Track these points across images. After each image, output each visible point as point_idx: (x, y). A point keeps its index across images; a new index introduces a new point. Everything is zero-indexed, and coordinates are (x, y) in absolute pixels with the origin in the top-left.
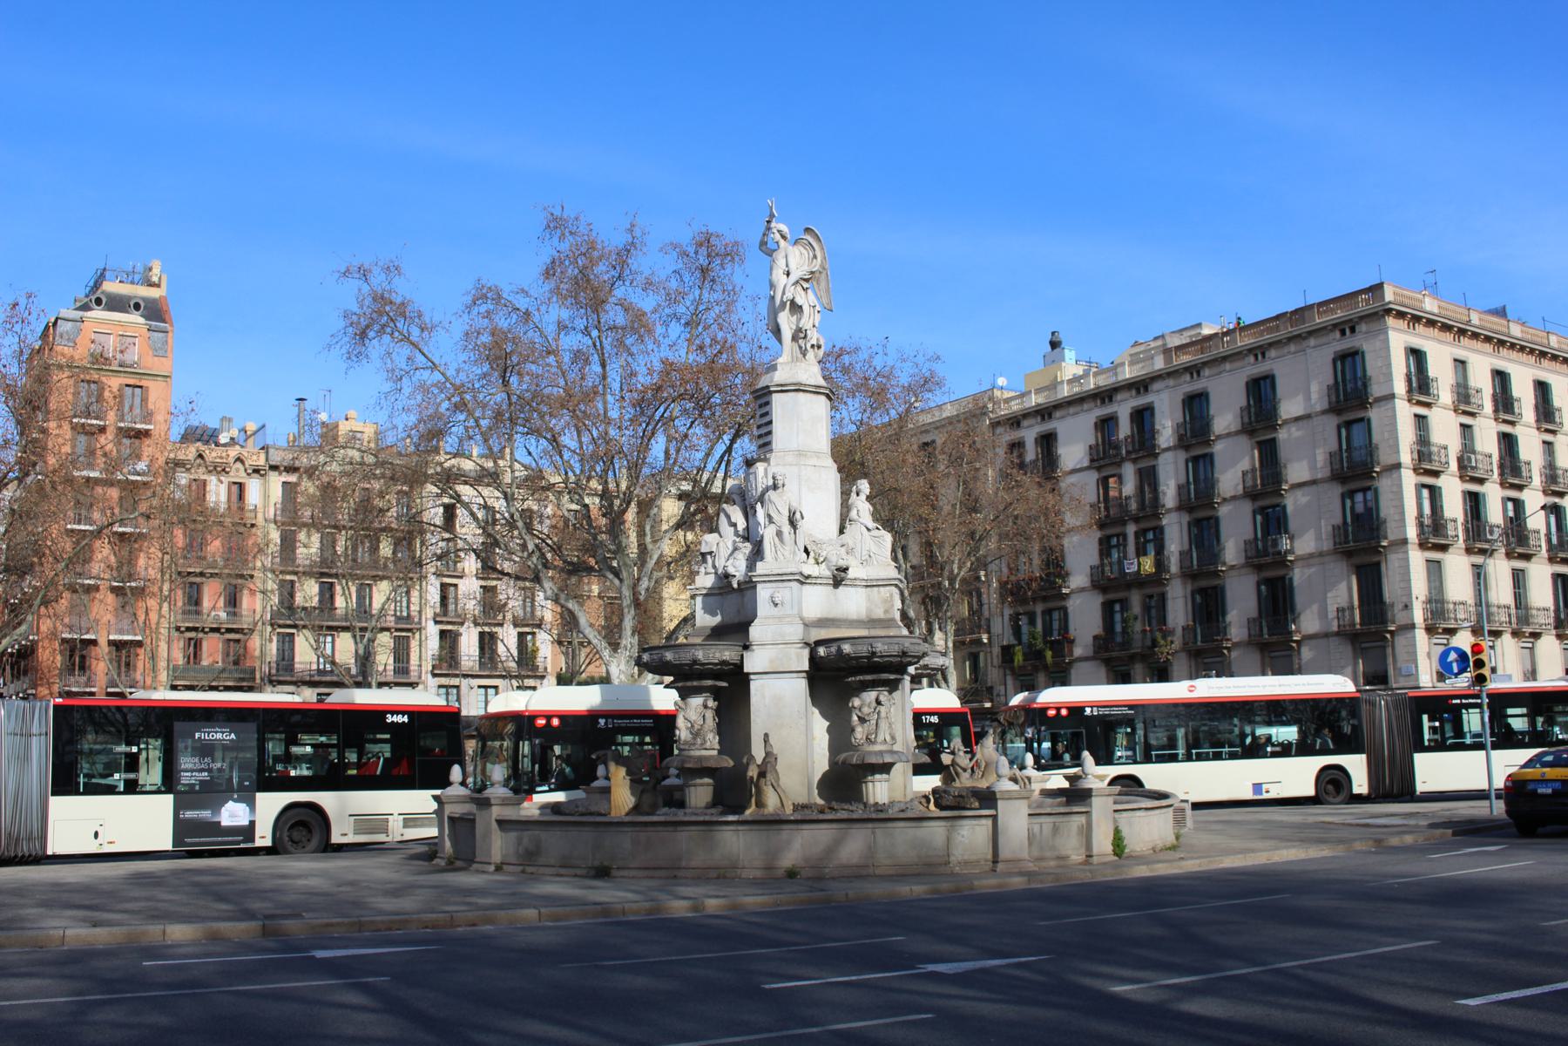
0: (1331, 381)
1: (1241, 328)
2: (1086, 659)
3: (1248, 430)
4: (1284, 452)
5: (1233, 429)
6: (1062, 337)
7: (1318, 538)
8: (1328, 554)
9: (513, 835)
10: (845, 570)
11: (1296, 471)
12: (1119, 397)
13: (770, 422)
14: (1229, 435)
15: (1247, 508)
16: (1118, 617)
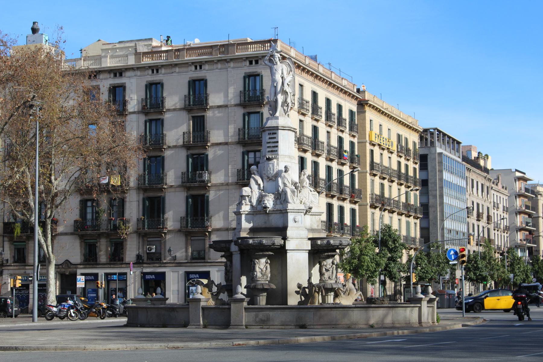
0: (242, 89)
1: (190, 49)
3: (188, 109)
4: (209, 124)
8: (232, 184)
9: (253, 314)
10: (310, 208)
11: (216, 136)
12: (102, 76)
13: (278, 142)
15: (183, 153)
16: (89, 210)
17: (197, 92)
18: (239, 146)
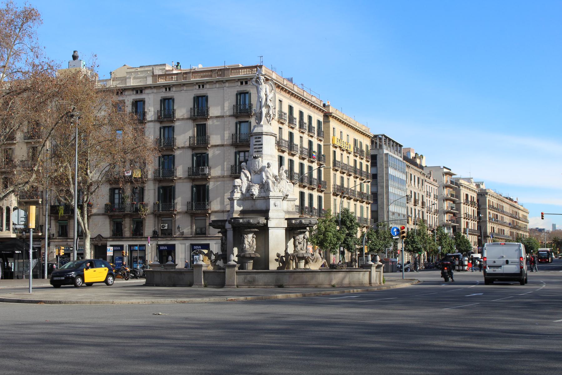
0: (235, 103)
2: (99, 215)
3: (193, 118)
4: (209, 131)
5: (186, 117)
6: (79, 54)
7: (223, 170)
8: (227, 177)
9: (242, 277)
10: (287, 196)
11: (214, 139)
13: (262, 144)
14: (183, 119)
15: (189, 153)
16: (117, 196)
17: (200, 107)
18: (232, 147)
